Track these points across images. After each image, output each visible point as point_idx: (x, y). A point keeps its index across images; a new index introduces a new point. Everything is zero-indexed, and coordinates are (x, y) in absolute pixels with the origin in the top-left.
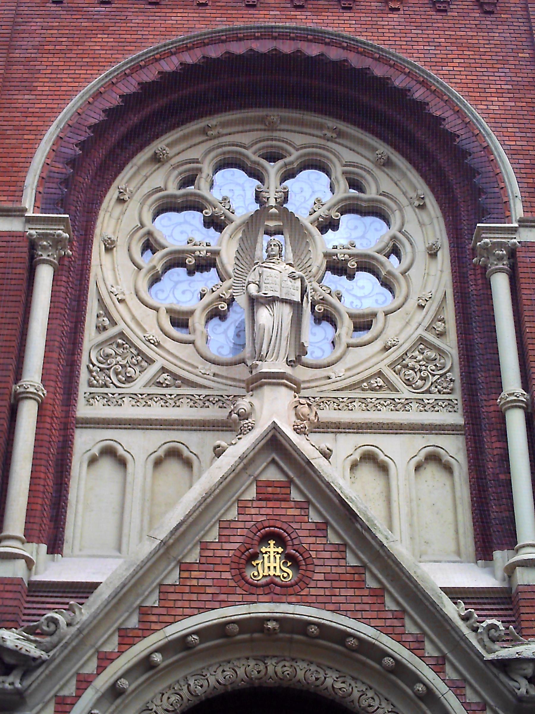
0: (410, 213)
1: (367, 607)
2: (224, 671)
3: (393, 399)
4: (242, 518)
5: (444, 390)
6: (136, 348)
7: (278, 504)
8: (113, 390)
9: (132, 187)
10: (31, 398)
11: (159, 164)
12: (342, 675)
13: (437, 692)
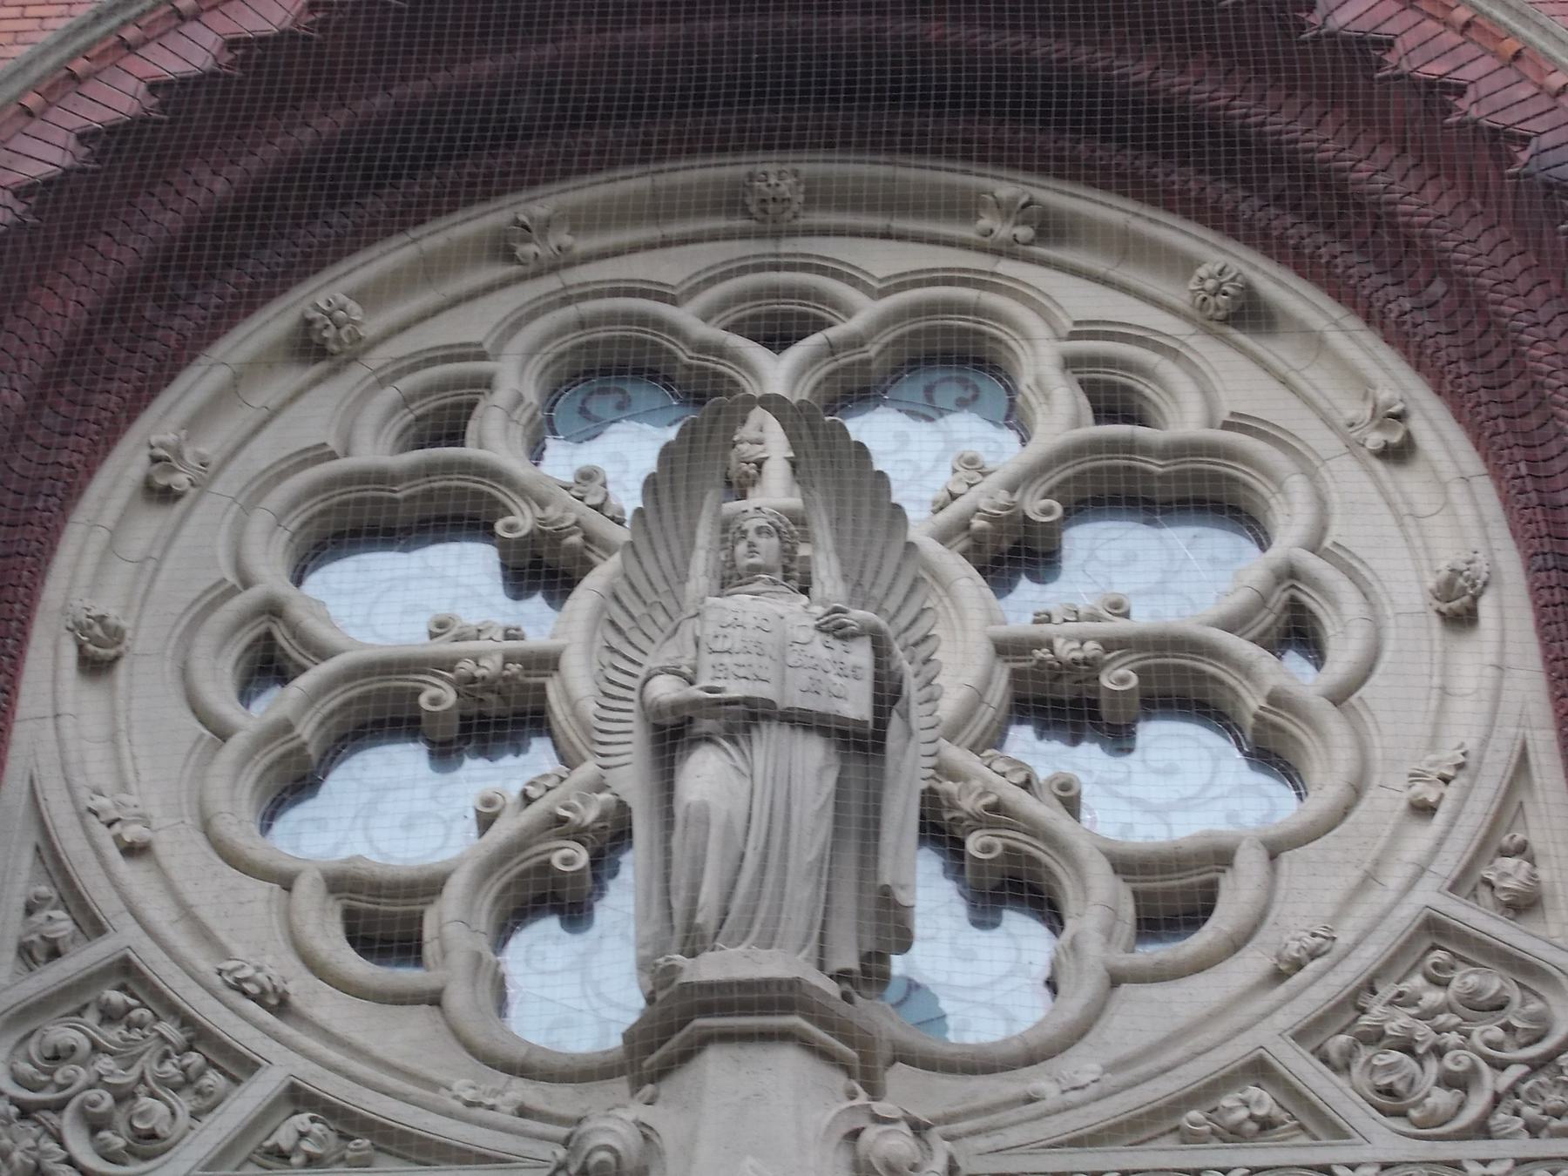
5: (1555, 1123)
6: (186, 1021)
9: (210, 446)
11: (322, 367)
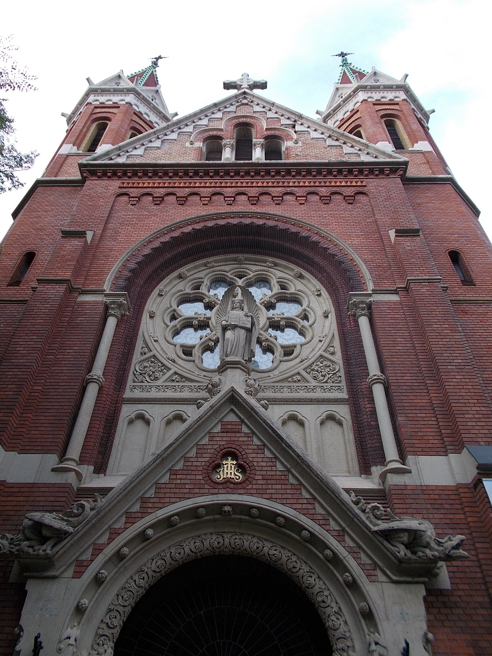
0: (313, 298)
1: (290, 496)
2: (195, 543)
3: (306, 387)
4: (211, 443)
6: (162, 363)
7: (234, 435)
8: (146, 384)
10: (94, 382)
12: (274, 545)
13: (340, 556)
